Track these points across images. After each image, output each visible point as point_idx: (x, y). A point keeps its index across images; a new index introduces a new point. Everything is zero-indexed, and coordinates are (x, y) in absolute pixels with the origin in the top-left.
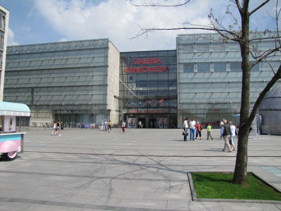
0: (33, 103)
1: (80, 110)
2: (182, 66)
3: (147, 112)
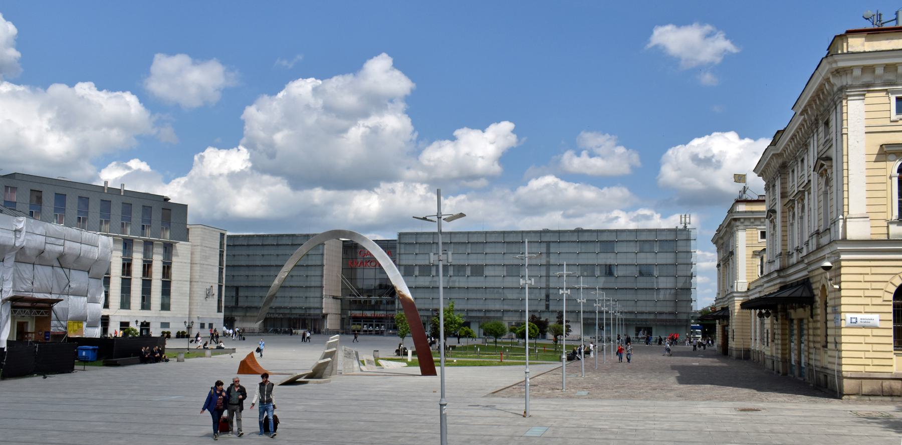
0: (237, 305)
1: (292, 314)
3: (373, 315)
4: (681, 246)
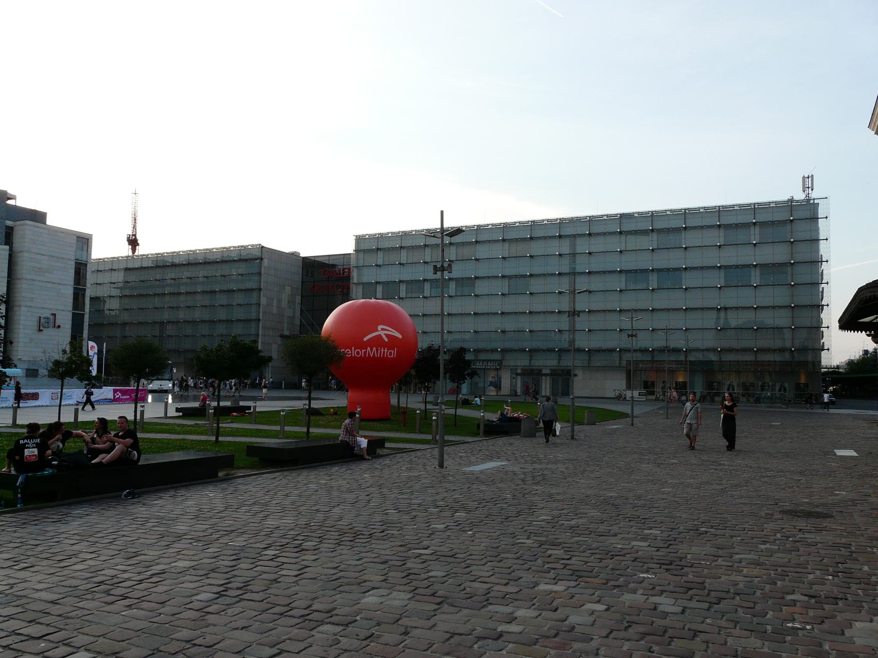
2: (360, 289)
4: (801, 231)
